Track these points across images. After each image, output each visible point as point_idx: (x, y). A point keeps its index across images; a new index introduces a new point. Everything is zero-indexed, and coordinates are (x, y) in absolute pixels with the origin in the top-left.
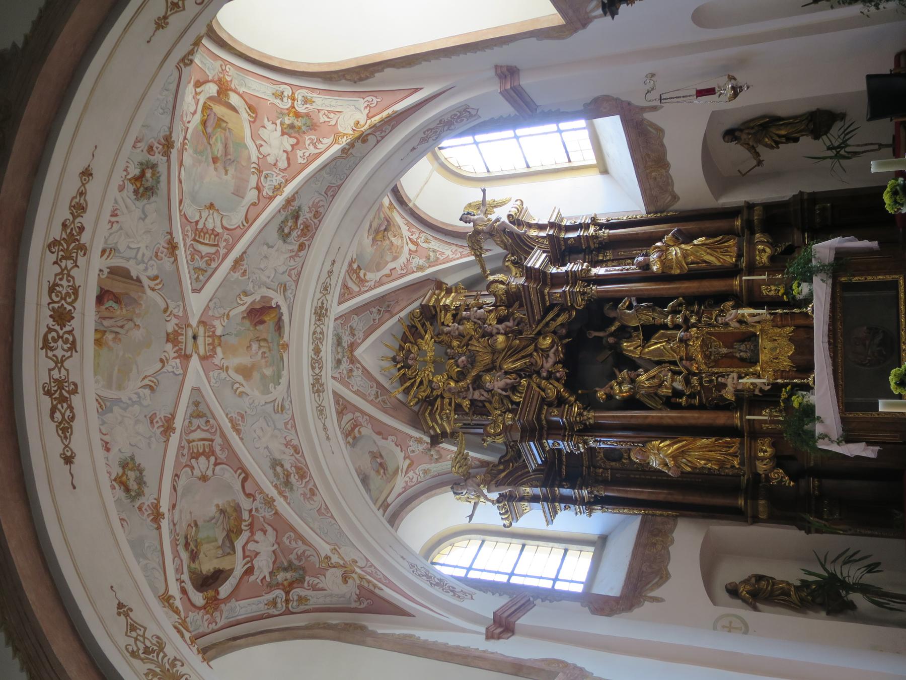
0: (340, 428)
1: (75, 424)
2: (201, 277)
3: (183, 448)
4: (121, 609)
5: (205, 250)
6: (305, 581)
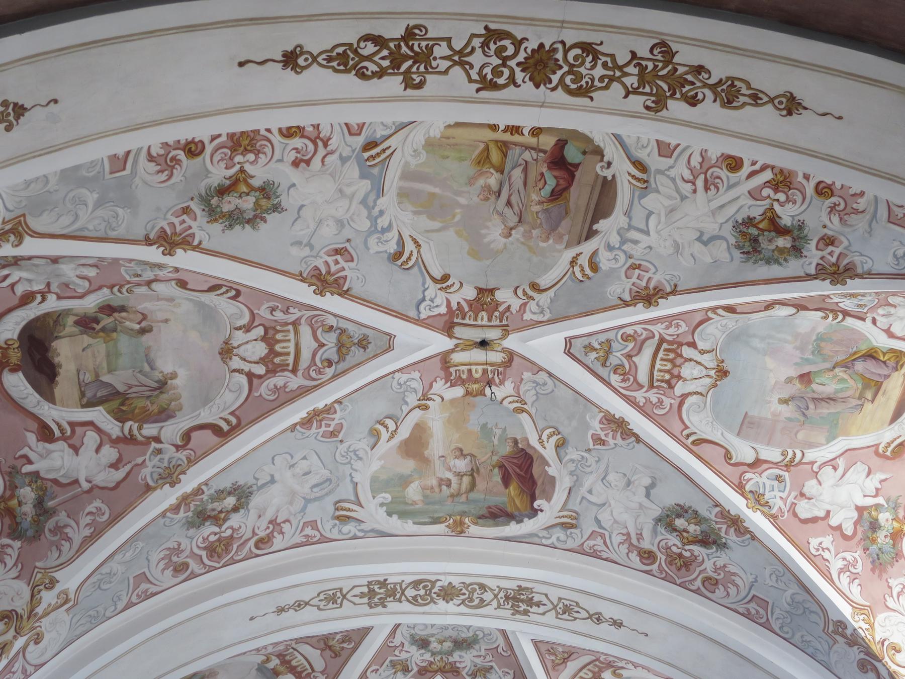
0: (298, 641)
1: (351, 79)
2: (593, 355)
3: (286, 311)
4: (13, 110)
5: (643, 361)
6: (14, 539)
